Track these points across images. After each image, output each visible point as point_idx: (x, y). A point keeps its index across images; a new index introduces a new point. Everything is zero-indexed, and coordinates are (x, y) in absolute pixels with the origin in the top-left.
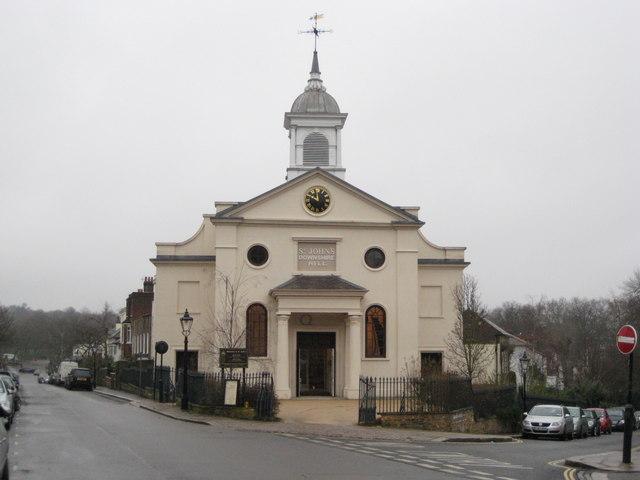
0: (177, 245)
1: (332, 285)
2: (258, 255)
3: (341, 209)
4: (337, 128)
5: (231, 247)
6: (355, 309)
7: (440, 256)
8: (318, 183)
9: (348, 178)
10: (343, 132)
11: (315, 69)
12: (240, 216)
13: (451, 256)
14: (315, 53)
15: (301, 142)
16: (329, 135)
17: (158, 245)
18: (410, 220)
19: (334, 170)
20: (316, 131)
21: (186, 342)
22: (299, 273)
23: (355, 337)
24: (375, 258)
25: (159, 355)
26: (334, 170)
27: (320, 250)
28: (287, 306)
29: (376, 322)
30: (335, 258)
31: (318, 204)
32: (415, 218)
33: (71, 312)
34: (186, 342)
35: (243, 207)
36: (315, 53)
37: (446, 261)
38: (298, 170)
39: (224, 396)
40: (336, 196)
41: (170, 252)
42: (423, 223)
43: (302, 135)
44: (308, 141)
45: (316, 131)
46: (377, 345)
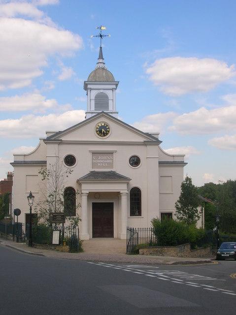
1: (112, 176)
2: (70, 160)
3: (116, 134)
5: (54, 155)
6: (123, 189)
8: (102, 121)
12: (60, 139)
14: (101, 48)
15: (93, 97)
16: (109, 93)
18: (154, 140)
19: (112, 113)
20: (101, 91)
21: (31, 209)
22: (93, 170)
23: (125, 203)
24: (135, 161)
25: (16, 216)
26: (112, 113)
28: (87, 188)
29: (136, 196)
31: (103, 131)
32: (157, 139)
34: (31, 209)
36: (101, 48)
38: (92, 113)
41: (21, 159)
43: (94, 94)
45: (101, 91)
46: (136, 208)
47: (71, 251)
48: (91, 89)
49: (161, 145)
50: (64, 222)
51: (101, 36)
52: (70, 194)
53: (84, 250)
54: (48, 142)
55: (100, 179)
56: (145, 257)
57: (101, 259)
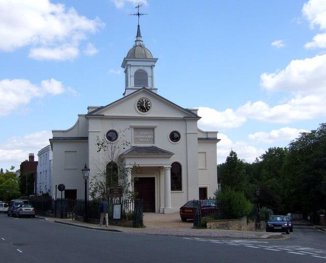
0: (63, 132)
1: (154, 151)
2: (112, 136)
3: (156, 111)
4: (152, 67)
6: (167, 164)
7: (204, 136)
8: (142, 96)
9: (159, 93)
10: (155, 69)
11: (139, 35)
13: (210, 136)
14: (139, 26)
16: (148, 70)
17: (53, 132)
18: (193, 116)
22: (135, 145)
24: (175, 137)
27: (146, 133)
28: (129, 163)
30: (154, 137)
31: (143, 107)
33: (306, 137)
35: (106, 108)
36: (139, 26)
37: (207, 139)
38: (132, 89)
39: (113, 215)
40: (154, 105)
42: (201, 118)
43: (132, 71)
44: (137, 73)
45: (141, 68)
46: (177, 184)
47: (135, 226)
48: (131, 66)
49: (199, 122)
50: (122, 196)
51: (139, 14)
52: (113, 170)
53: (145, 223)
54: (90, 117)
55: (144, 153)
56: (214, 232)
57: (193, 235)
